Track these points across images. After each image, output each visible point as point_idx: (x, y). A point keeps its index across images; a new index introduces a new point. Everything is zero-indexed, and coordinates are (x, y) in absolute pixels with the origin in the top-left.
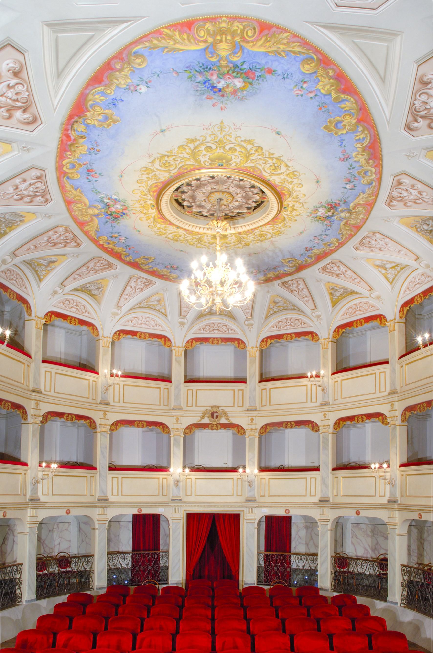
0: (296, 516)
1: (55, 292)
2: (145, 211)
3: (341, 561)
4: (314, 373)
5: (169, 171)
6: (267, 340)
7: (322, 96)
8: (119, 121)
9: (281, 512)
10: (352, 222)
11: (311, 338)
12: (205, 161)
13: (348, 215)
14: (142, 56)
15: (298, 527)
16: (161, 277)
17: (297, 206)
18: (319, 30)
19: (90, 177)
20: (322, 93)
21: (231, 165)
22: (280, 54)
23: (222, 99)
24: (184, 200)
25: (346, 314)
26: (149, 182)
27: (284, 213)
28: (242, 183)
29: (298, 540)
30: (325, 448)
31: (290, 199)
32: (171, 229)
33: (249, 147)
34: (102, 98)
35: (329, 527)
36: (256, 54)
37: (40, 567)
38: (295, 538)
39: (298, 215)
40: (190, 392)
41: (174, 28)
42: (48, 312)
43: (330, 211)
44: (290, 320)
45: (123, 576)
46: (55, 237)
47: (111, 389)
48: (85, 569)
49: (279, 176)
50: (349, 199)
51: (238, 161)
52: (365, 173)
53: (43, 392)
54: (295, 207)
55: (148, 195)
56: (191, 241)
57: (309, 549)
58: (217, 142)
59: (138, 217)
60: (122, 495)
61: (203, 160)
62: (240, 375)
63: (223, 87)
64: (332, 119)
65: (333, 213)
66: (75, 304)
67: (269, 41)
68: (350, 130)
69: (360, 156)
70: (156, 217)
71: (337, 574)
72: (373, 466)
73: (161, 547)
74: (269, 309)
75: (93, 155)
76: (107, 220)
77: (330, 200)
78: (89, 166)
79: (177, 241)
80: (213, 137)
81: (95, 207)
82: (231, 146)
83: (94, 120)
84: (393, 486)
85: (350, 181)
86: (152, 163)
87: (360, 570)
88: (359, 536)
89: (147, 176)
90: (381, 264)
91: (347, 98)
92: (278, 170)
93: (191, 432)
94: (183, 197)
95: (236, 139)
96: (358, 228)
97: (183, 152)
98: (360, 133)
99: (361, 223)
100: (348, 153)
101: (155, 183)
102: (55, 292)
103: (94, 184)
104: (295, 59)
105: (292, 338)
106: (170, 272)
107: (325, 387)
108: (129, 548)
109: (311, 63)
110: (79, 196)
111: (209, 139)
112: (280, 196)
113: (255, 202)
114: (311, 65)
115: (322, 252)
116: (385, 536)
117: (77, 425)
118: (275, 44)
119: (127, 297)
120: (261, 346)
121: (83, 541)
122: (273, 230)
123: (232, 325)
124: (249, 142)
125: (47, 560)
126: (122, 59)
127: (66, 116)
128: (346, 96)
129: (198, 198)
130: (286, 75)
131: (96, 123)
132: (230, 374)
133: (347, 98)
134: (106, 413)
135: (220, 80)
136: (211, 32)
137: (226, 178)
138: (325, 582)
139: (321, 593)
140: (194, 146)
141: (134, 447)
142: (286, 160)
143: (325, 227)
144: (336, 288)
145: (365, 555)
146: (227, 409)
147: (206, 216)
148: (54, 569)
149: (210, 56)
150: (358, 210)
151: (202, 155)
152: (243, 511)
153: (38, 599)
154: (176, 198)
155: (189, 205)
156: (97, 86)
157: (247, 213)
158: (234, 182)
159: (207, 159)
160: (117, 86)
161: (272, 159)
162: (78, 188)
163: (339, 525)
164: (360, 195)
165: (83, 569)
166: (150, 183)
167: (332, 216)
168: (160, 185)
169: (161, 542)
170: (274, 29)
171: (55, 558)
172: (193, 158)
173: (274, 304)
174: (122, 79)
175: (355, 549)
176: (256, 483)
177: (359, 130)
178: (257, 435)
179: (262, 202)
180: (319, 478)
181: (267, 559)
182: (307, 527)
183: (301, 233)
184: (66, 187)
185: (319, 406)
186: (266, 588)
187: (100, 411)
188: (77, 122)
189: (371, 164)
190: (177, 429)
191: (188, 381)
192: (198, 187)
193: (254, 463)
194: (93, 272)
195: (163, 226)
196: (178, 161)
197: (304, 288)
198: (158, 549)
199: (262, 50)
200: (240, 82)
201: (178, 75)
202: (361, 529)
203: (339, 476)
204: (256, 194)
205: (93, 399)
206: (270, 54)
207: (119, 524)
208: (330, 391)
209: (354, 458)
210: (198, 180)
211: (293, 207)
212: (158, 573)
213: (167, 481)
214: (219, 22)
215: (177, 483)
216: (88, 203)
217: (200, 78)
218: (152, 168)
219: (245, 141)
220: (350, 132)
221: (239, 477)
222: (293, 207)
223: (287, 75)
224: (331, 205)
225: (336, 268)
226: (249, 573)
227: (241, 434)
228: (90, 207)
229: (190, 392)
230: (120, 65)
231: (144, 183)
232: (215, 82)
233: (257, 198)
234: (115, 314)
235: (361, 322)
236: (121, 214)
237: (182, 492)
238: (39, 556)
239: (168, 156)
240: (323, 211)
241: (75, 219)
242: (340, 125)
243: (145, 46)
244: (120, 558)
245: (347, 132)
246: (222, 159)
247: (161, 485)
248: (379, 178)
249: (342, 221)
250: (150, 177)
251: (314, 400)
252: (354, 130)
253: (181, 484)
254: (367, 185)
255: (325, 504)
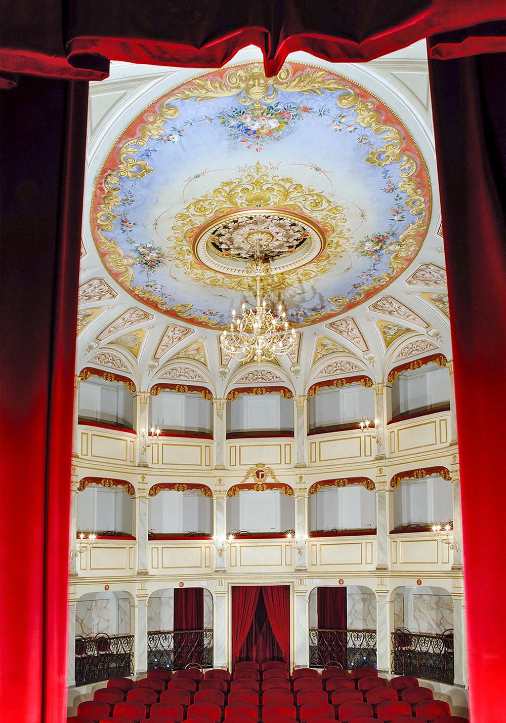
0: (351, 587)
1: (91, 347)
2: (181, 258)
3: (402, 638)
4: (368, 423)
5: (205, 215)
6: (316, 387)
7: (363, 129)
8: (152, 171)
9: (334, 583)
10: (403, 254)
11: (364, 383)
12: (242, 203)
13: (398, 248)
14: (174, 107)
15: (354, 599)
16: (200, 324)
17: (342, 241)
18: (356, 67)
19: (124, 228)
20: (362, 127)
21: (269, 204)
22: (315, 92)
23: (257, 141)
24: (221, 243)
25: (402, 354)
26: (184, 228)
27: (328, 250)
28: (281, 221)
29: (354, 615)
30: (382, 508)
31: (334, 235)
32: (209, 274)
33: (287, 185)
34: (135, 150)
35: (388, 599)
36: (291, 94)
37: (78, 649)
38: (351, 612)
39: (343, 251)
40: (233, 449)
41: (206, 78)
42: (84, 369)
43: (378, 245)
44: (341, 364)
45: (165, 658)
46: (90, 290)
47: (149, 450)
48: (125, 651)
49: (321, 213)
50: (397, 231)
51: (277, 200)
52: (414, 203)
53: (80, 456)
54: (340, 243)
55: (184, 241)
56: (230, 284)
57: (367, 625)
58: (253, 183)
59: (175, 264)
60: (163, 568)
61: (239, 202)
62: (287, 427)
63: (258, 129)
64: (374, 150)
65: (381, 247)
66: (111, 358)
67: (304, 81)
68: (394, 160)
69: (407, 186)
70: (193, 263)
71: (398, 653)
72: (434, 528)
73: (205, 626)
74: (317, 353)
75: (127, 205)
76: (143, 269)
77: (377, 233)
78: (123, 217)
79: (216, 285)
80: (249, 178)
81: (130, 257)
82: (270, 185)
83: (127, 172)
84: (457, 551)
85: (397, 212)
86: (188, 208)
87: (424, 649)
88: (422, 609)
89: (182, 222)
90: (437, 298)
91: (389, 129)
92: (320, 206)
93: (235, 494)
94: (221, 240)
95: (274, 178)
96: (410, 261)
97: (219, 195)
98: (406, 162)
99: (413, 255)
100: (393, 184)
101: (191, 229)
102: (91, 347)
103: (129, 235)
104: (331, 95)
105: (343, 384)
106: (209, 319)
107: (380, 439)
108: (170, 627)
109: (349, 98)
110: (114, 247)
111: (245, 181)
112: (323, 233)
113: (297, 240)
114: (348, 100)
115: (372, 288)
116: (451, 609)
117: (114, 491)
118: (310, 83)
119: (164, 347)
120: (309, 395)
121: (122, 621)
122: (317, 268)
123: (276, 372)
124: (287, 180)
125: (85, 642)
126: (154, 112)
127: (100, 170)
128: (387, 127)
129: (236, 240)
130: (323, 111)
131: (130, 174)
132: (276, 425)
133: (389, 129)
134: (145, 476)
135: (254, 122)
136: (244, 78)
137: (264, 218)
138: (385, 663)
139: (380, 675)
140: (229, 189)
141: (174, 512)
142: (327, 196)
143: (374, 262)
144: (389, 326)
145: (429, 632)
146: (272, 467)
147: (245, 258)
148: (92, 652)
149: (243, 100)
150: (408, 242)
151: (238, 196)
152: (293, 582)
153: (77, 685)
154: (213, 242)
155: (227, 247)
156: (129, 139)
157: (288, 251)
158: (273, 221)
159: (244, 201)
160: (150, 137)
161: (312, 195)
162: (112, 240)
163: (399, 596)
164: (409, 226)
165: (122, 652)
166: (186, 229)
167: (380, 249)
168: (197, 231)
169: (205, 620)
170: (308, 69)
171: (93, 639)
172: (230, 201)
173: (322, 347)
174: (155, 130)
175: (419, 625)
176: (306, 549)
177: (404, 160)
178: (306, 495)
179: (305, 240)
180: (375, 543)
181: (321, 637)
182: (364, 600)
183: (348, 269)
184: (101, 239)
185: (374, 460)
186: (320, 671)
187: (139, 474)
188: (110, 175)
189: (419, 193)
190: (220, 491)
191: (231, 435)
192: (236, 229)
193: (304, 526)
194: (129, 323)
195: (200, 272)
196: (213, 204)
197: (354, 328)
198: (201, 627)
199: (297, 90)
200: (275, 123)
201: (211, 122)
202: (424, 601)
203: (398, 540)
204: (297, 232)
205: (131, 462)
206: (305, 93)
207: (160, 600)
208: (386, 443)
209: (415, 519)
210: (235, 222)
211: (337, 243)
212: (204, 655)
213: (210, 550)
214: (251, 68)
215: (221, 552)
216: (122, 254)
217: (234, 123)
218: (187, 213)
219: (283, 180)
220: (395, 163)
221: (288, 544)
222: (337, 243)
223: (324, 111)
224: (378, 238)
225: (388, 305)
226: (300, 654)
227: (289, 494)
228: (124, 258)
229: (233, 449)
230: (152, 118)
231: (180, 230)
232: (249, 125)
233: (298, 235)
234: (152, 367)
235: (419, 363)
236: (157, 262)
237: (225, 564)
238: (77, 638)
239: (203, 201)
240: (371, 245)
241: (110, 271)
242: (383, 156)
243: (177, 98)
244: (161, 639)
245: (391, 162)
246: (260, 200)
247: (203, 555)
248: (429, 207)
249: (392, 254)
250: (186, 223)
251: (368, 453)
252: (398, 159)
253: (225, 553)
254: (416, 215)
255: (383, 573)
